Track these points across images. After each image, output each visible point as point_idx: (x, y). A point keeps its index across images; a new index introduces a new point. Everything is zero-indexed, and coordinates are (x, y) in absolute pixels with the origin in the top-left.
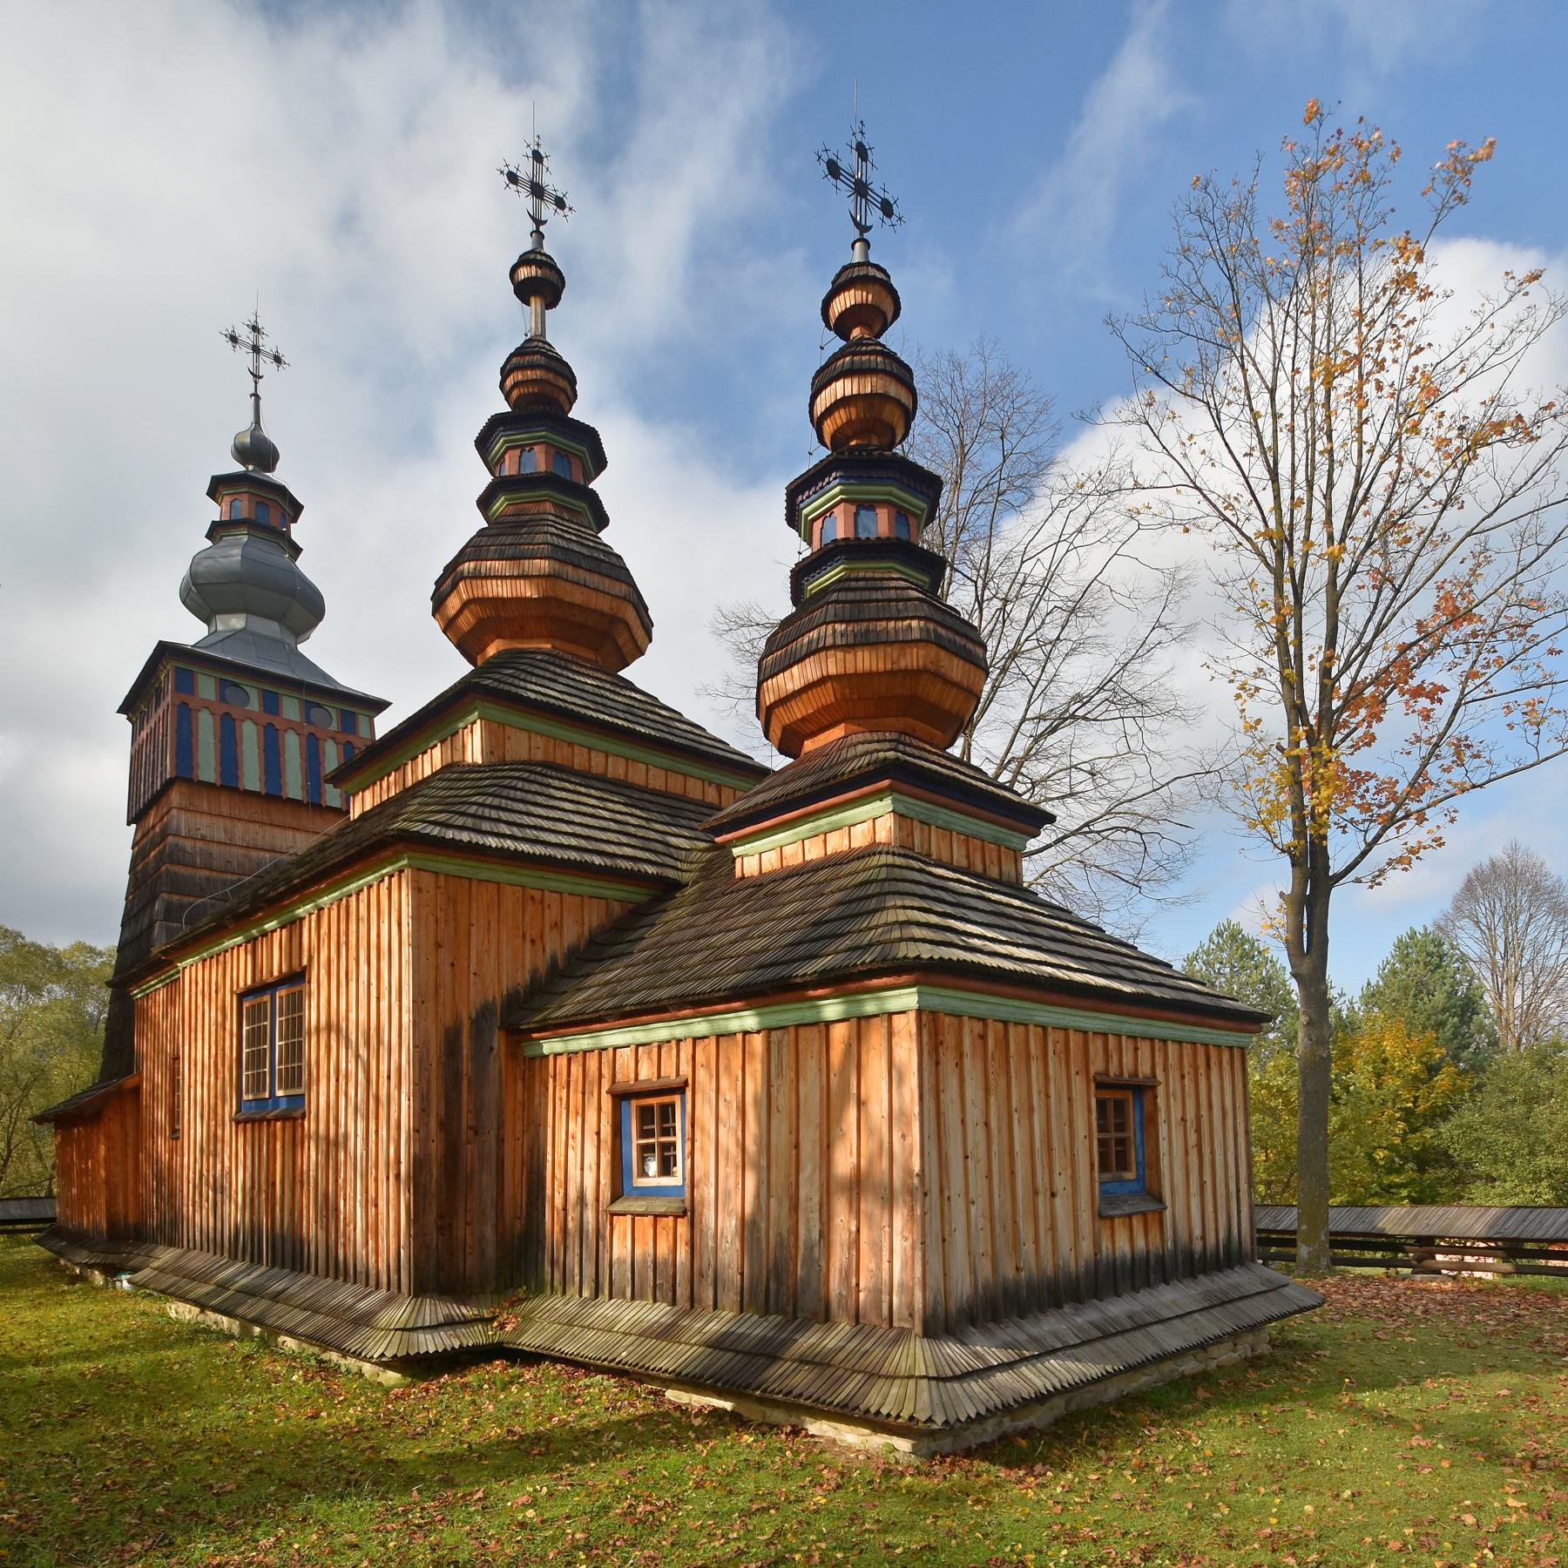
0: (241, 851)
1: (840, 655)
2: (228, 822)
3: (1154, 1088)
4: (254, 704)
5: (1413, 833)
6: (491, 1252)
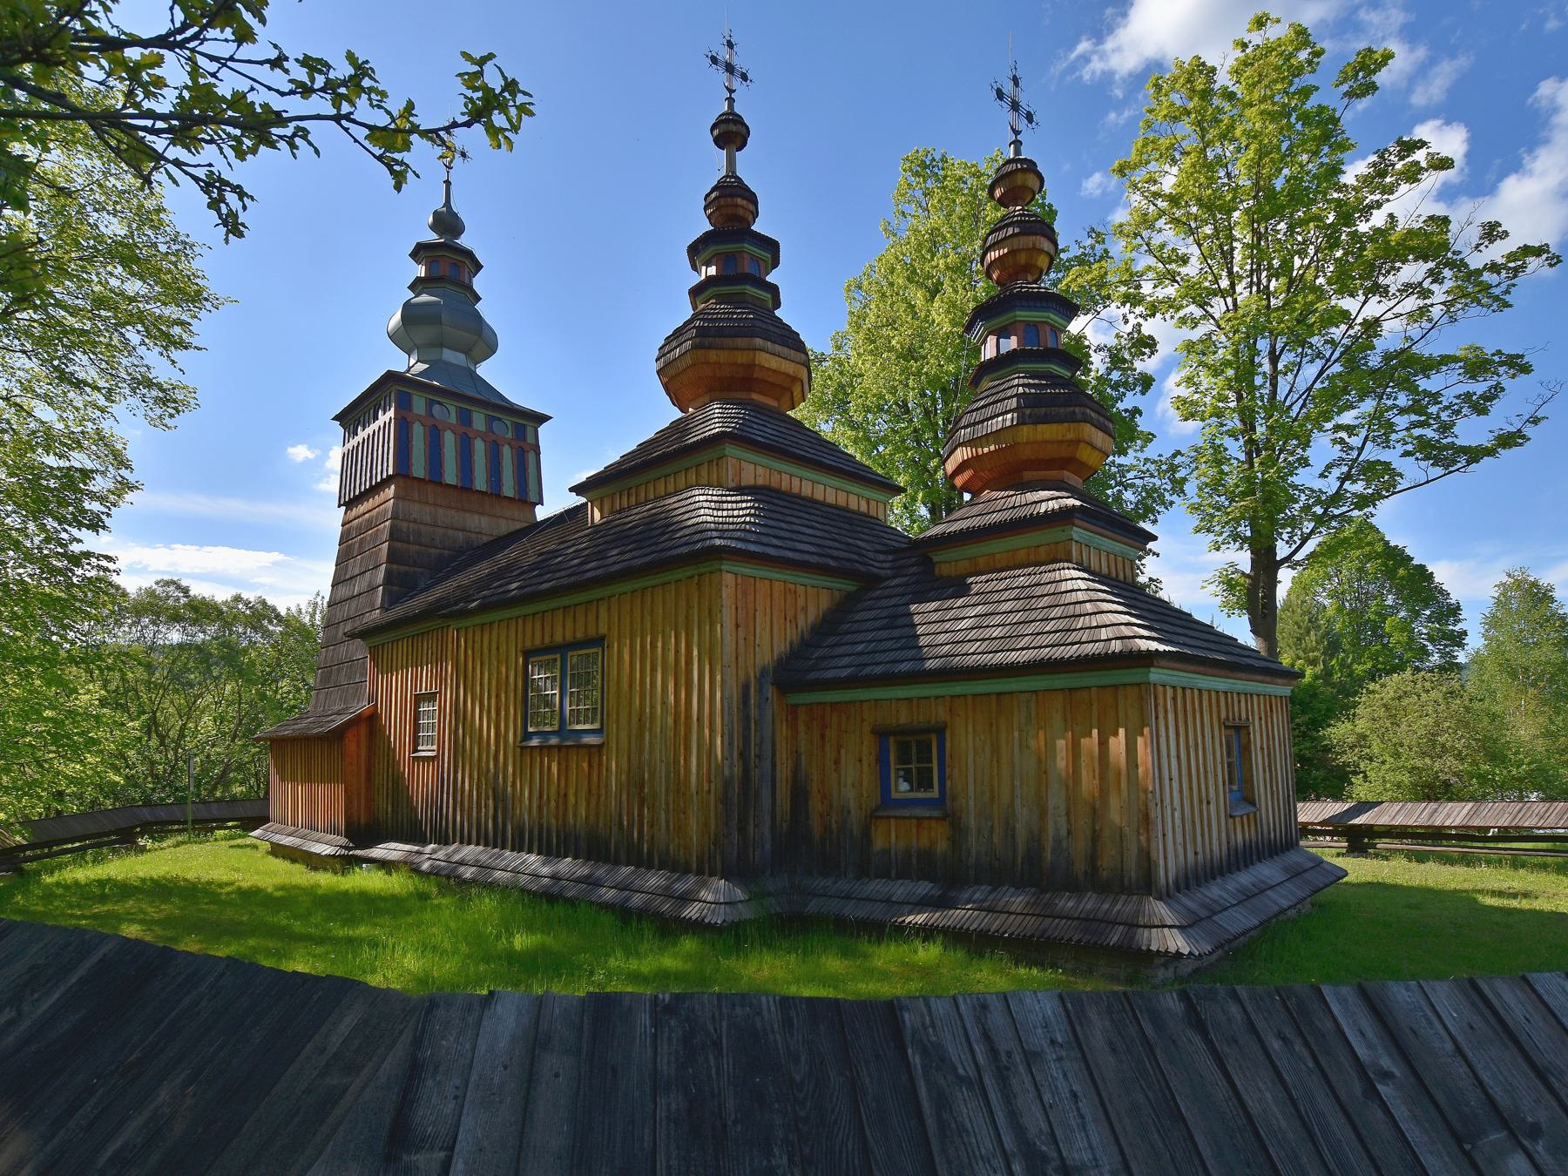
6: (768, 846)
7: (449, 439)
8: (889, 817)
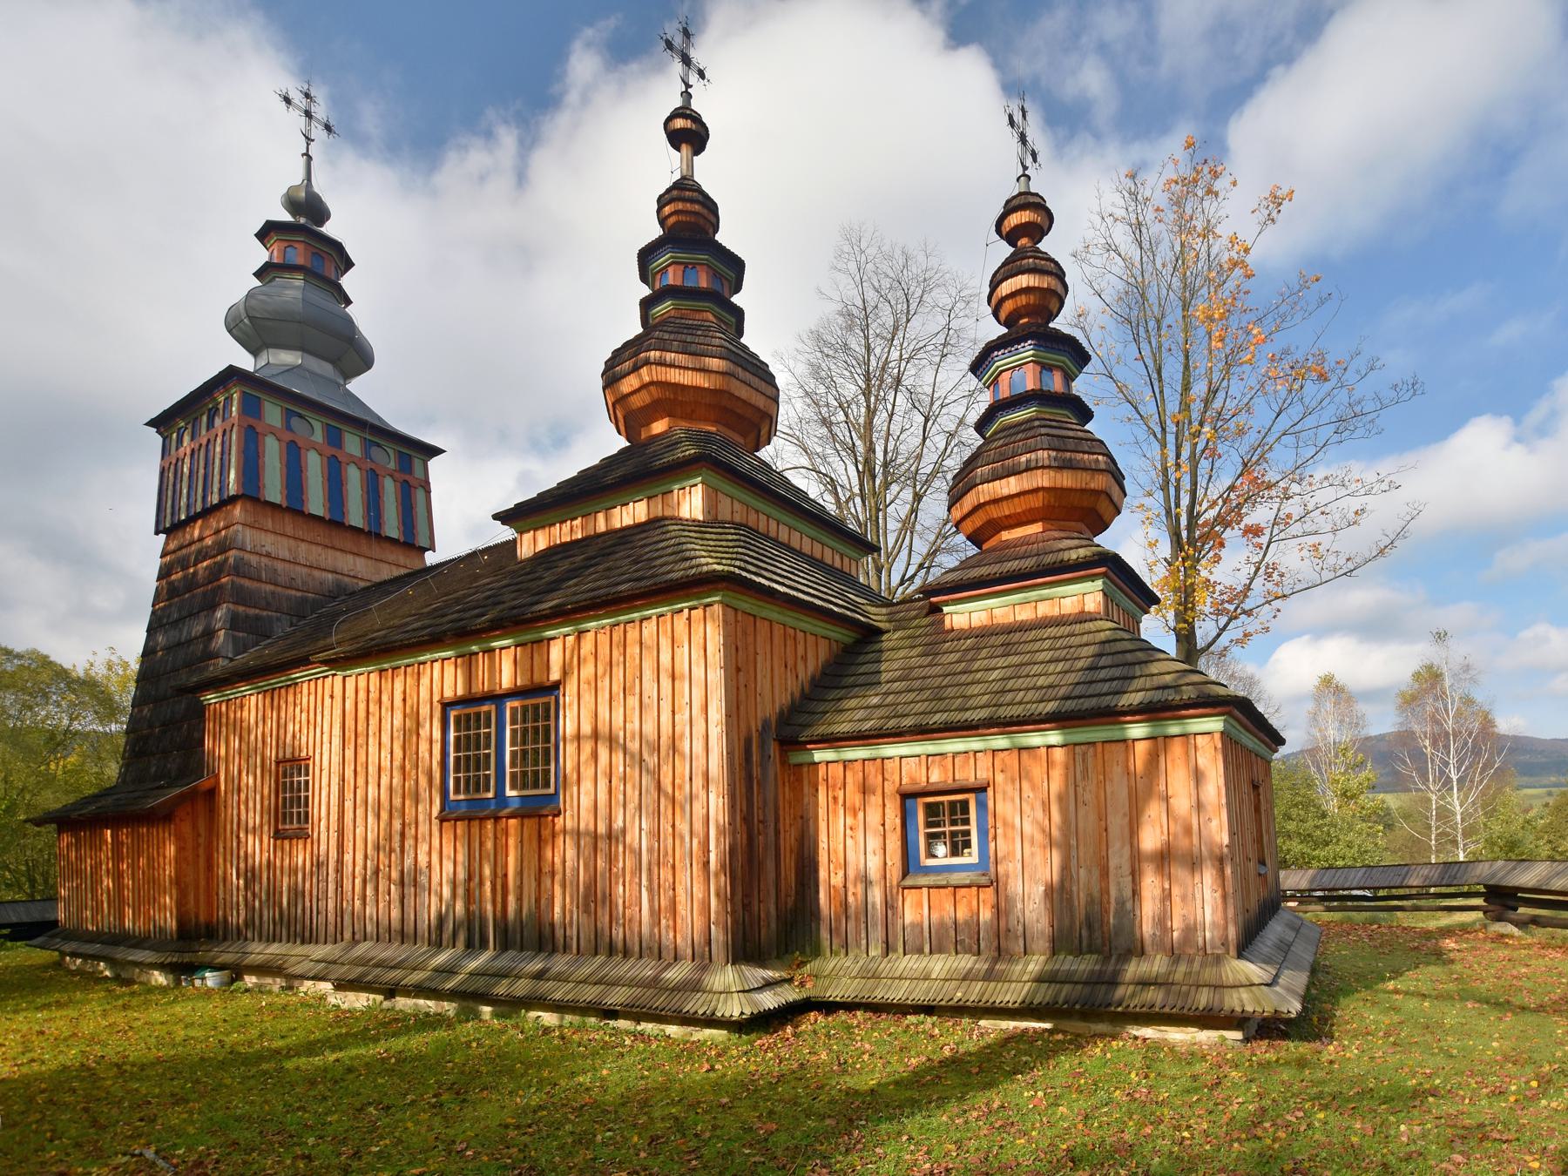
0: (305, 570)
1: (1052, 473)
2: (292, 542)
4: (319, 436)
5: (1251, 624)
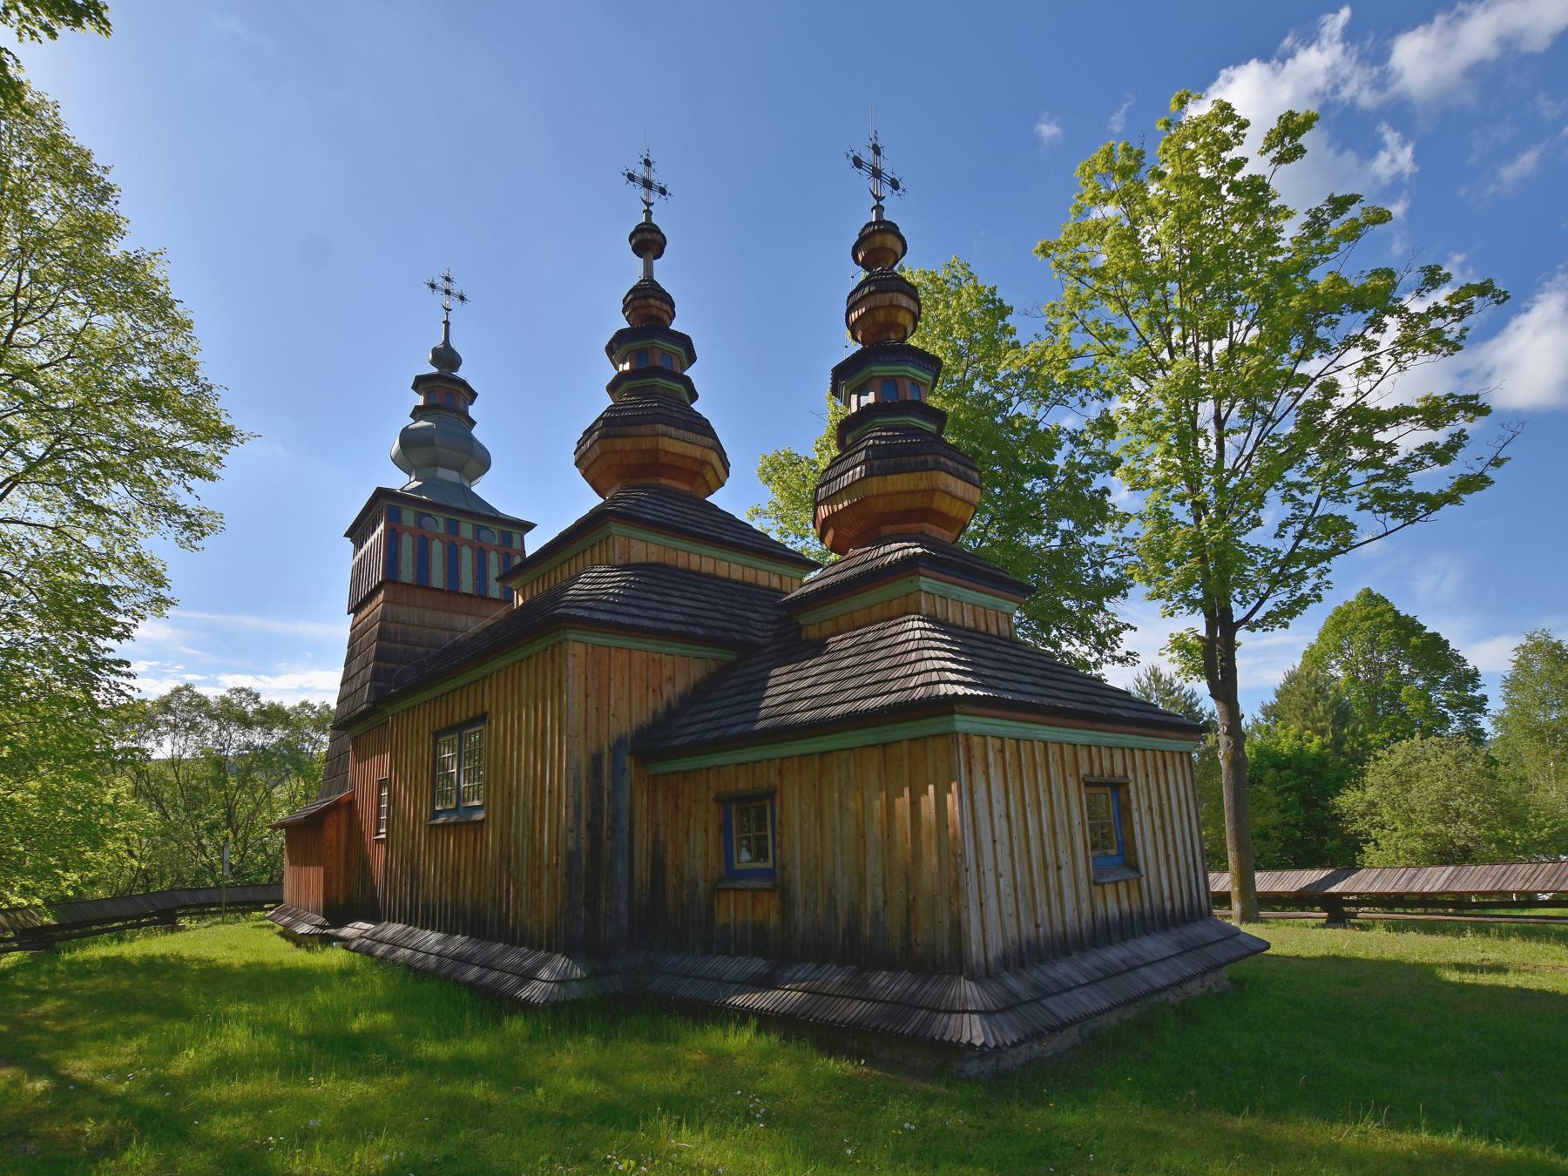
3: (1126, 785)
7: (437, 548)
8: (728, 890)
